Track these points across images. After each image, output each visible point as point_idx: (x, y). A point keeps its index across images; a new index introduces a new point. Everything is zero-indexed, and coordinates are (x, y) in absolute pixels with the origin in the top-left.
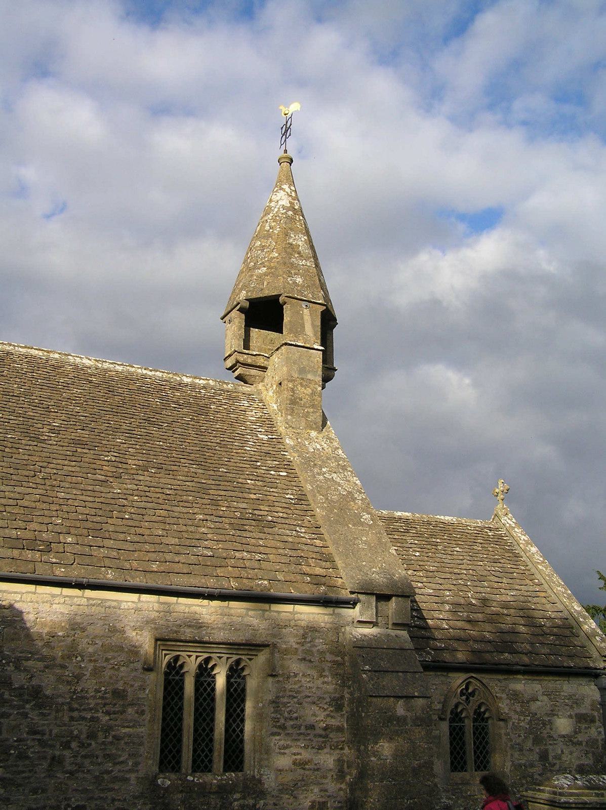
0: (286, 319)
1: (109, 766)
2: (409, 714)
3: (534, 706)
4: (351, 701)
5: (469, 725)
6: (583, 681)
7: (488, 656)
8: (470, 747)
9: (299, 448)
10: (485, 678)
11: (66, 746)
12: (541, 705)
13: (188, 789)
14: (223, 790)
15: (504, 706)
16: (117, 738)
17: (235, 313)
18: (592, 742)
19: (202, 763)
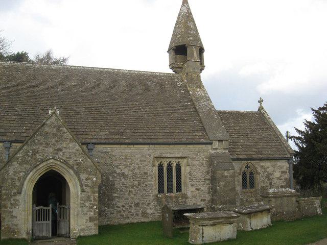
0: (188, 52)
1: (144, 192)
2: (228, 175)
3: (268, 170)
4: (212, 172)
5: (248, 176)
6: (284, 161)
7: (254, 156)
8: (248, 182)
9: (194, 95)
10: (253, 162)
11: (133, 188)
12: (270, 170)
13: (166, 197)
14: (176, 197)
15: (259, 170)
16: (146, 185)
17: (171, 51)
18: (286, 179)
19: (170, 190)
